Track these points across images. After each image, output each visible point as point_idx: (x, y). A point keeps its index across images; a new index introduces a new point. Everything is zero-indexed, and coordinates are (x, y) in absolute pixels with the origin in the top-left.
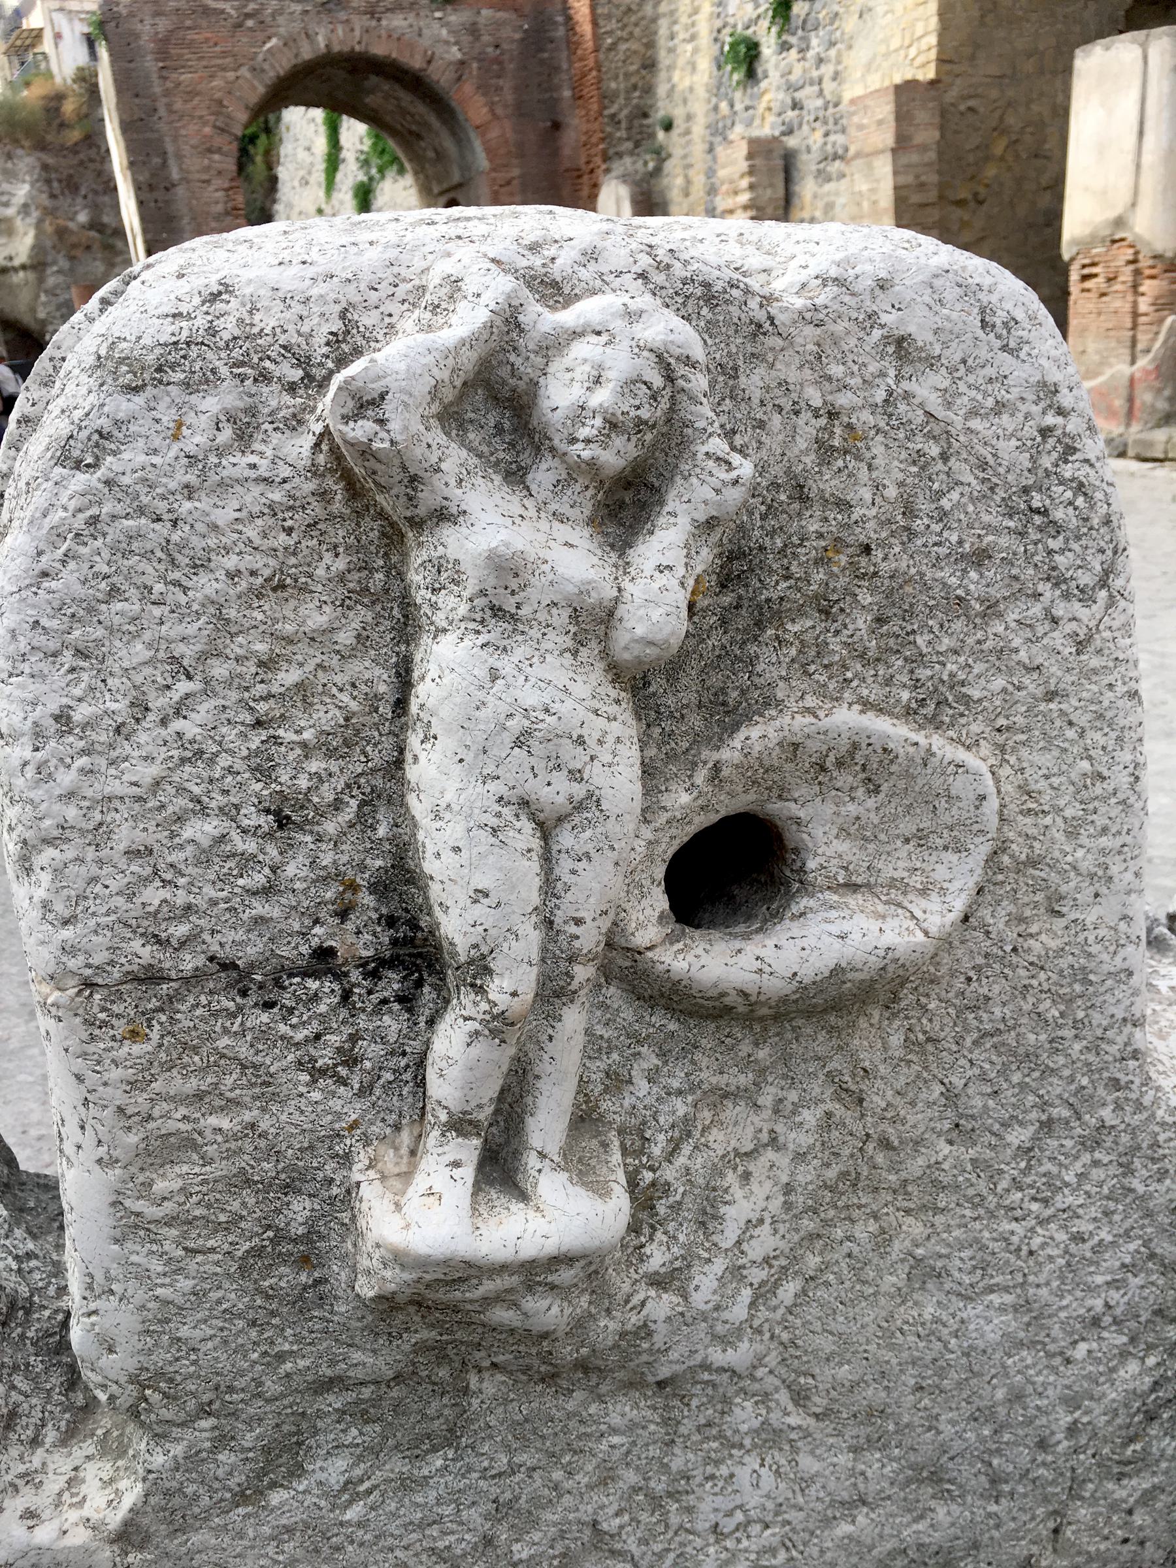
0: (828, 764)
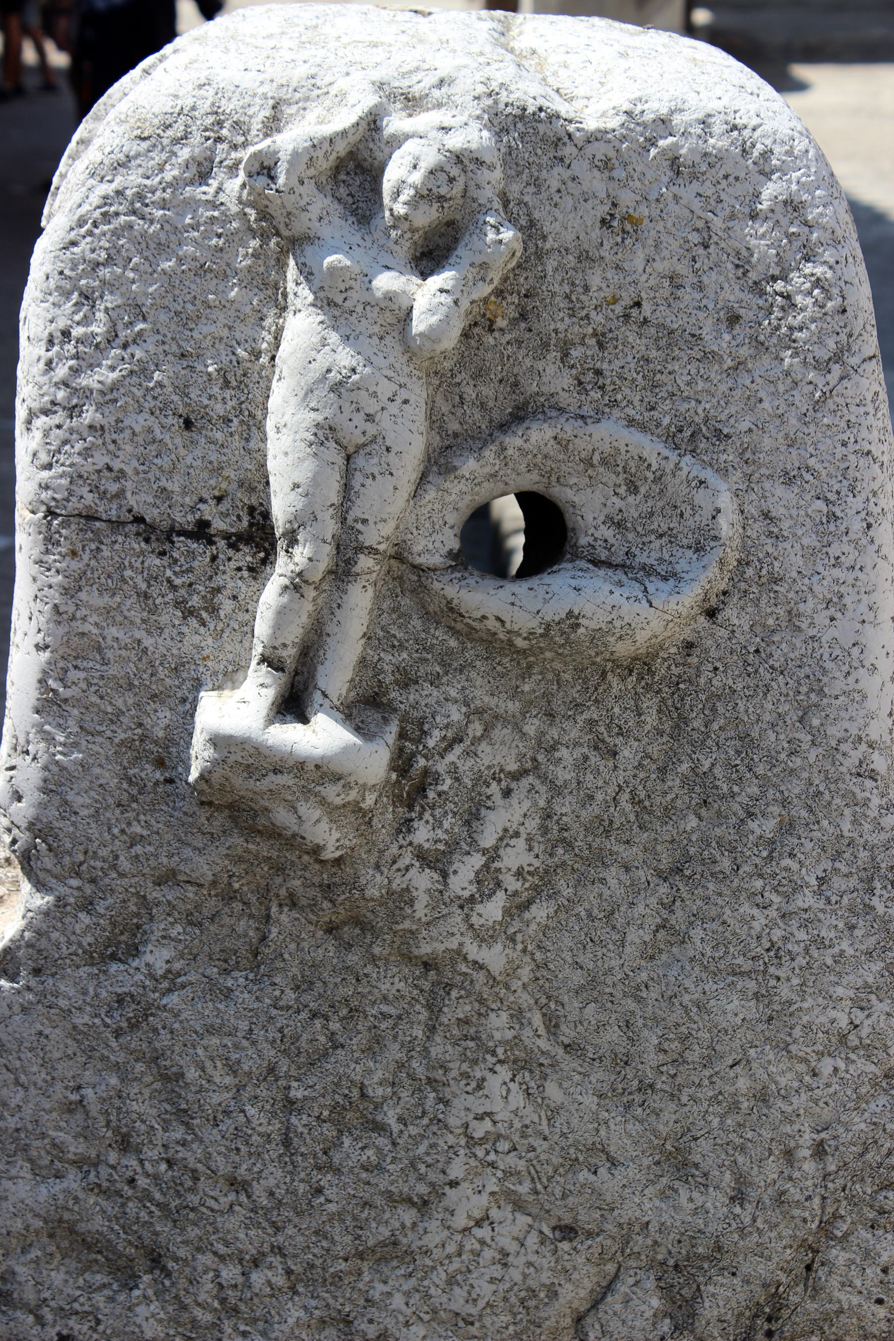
0: (595, 462)
